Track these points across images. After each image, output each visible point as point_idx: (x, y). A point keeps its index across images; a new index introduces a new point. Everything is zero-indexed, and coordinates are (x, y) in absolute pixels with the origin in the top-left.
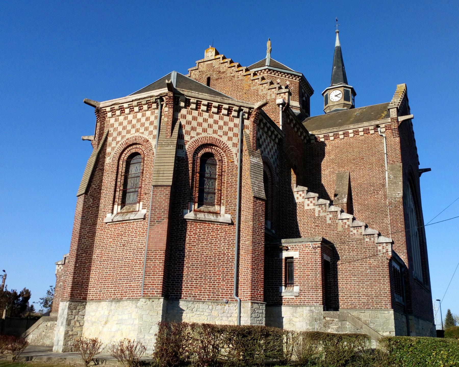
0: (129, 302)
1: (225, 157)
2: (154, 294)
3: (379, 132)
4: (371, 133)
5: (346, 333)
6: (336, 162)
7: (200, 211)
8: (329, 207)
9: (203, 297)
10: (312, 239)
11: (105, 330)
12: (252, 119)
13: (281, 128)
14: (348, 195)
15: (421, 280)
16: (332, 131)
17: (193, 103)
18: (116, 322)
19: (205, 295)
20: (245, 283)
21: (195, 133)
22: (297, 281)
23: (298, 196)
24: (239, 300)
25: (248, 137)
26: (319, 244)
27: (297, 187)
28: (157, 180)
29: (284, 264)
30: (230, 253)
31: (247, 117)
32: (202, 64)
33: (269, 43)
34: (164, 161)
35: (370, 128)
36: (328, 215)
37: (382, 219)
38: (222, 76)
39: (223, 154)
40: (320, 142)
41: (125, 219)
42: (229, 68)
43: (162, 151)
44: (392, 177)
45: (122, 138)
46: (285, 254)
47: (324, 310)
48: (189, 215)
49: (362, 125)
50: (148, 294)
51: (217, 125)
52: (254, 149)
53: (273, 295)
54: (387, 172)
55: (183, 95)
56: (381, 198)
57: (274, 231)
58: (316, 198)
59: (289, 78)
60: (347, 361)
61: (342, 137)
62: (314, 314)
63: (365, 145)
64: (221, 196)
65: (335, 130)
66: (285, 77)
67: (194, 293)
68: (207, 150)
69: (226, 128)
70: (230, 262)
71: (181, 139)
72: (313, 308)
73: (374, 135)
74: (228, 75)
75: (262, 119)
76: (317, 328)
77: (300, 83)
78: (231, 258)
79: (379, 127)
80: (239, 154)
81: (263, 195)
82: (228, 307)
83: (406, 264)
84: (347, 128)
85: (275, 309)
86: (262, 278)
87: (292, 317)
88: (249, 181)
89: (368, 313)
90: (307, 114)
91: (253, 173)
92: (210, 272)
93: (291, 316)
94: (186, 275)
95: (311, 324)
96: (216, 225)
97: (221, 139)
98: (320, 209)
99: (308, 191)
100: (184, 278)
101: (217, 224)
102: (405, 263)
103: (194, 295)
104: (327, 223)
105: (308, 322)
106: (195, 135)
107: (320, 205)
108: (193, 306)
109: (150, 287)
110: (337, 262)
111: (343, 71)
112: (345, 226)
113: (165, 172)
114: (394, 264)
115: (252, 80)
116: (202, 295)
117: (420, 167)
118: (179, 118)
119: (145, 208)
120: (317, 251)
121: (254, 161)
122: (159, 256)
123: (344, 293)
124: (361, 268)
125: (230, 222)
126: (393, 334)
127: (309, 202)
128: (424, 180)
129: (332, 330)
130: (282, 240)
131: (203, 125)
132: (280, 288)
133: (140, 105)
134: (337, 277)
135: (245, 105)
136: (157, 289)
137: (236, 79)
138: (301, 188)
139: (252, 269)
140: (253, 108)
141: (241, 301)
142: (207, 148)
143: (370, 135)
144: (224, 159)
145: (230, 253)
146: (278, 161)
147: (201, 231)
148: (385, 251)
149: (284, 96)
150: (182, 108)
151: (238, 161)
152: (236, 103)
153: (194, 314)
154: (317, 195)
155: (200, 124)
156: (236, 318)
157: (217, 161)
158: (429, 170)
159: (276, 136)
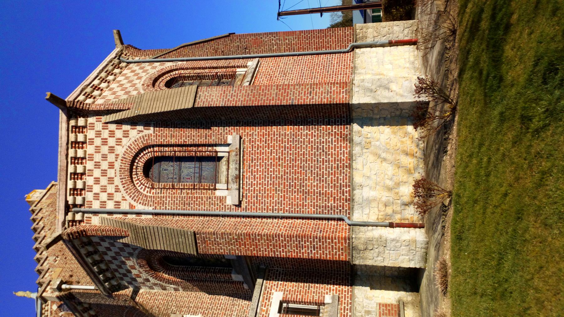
33: (20, 294)
45: (117, 190)
97: (121, 155)
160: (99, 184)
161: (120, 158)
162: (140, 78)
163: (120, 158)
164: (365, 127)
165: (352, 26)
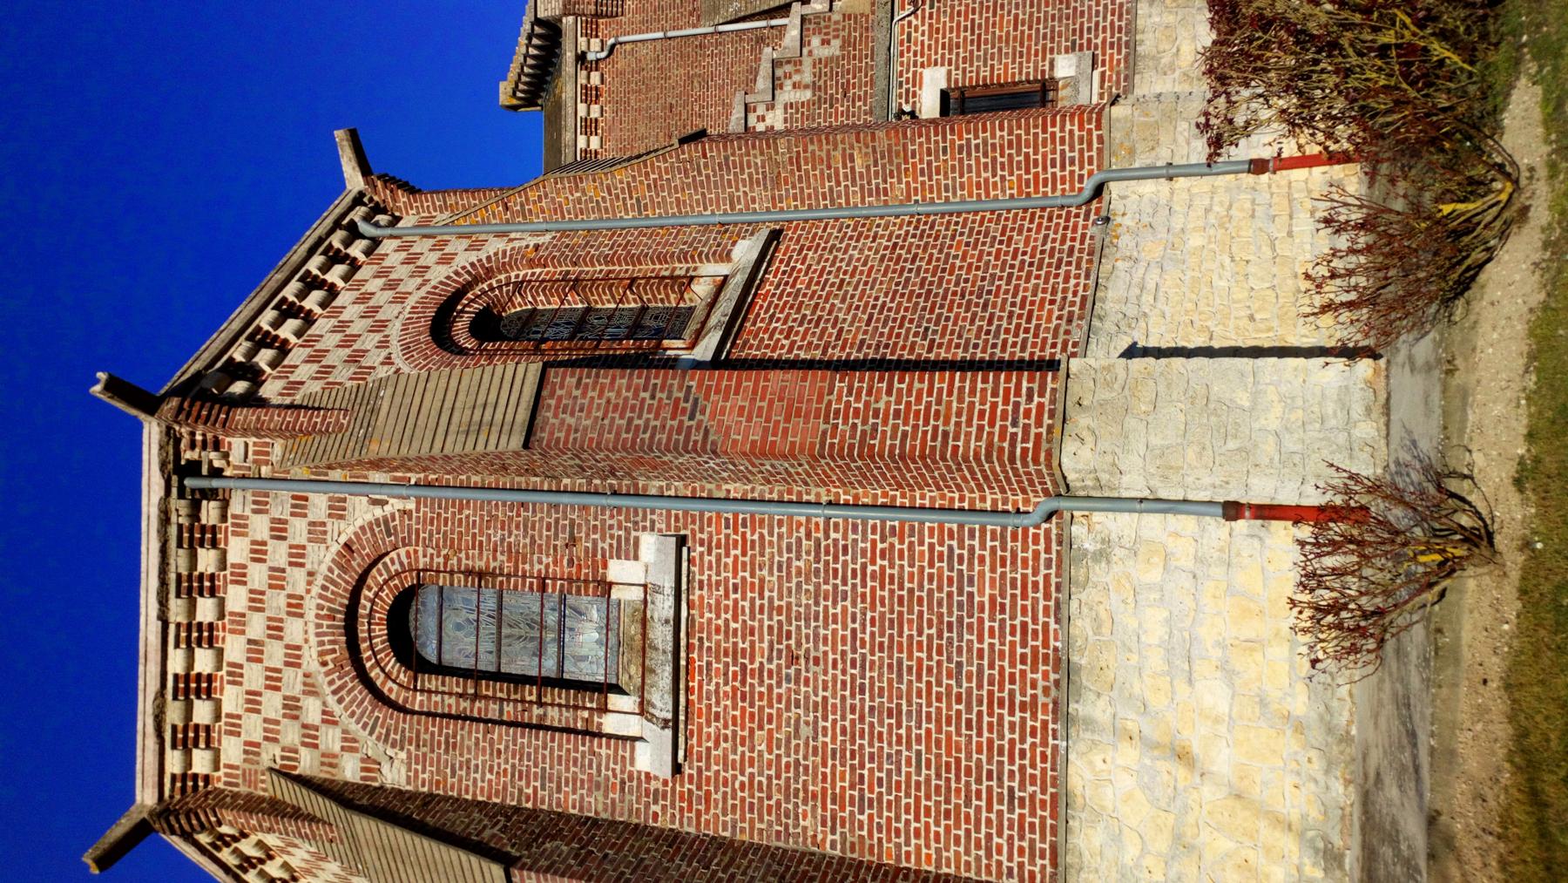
0: (1074, 604)
2: (1041, 406)
11: (1222, 760)
18: (1182, 688)
22: (1036, 63)
28: (506, 428)
34: (434, 414)
35: (582, 80)
36: (810, 53)
41: (670, 648)
43: (387, 436)
45: (311, 690)
50: (1038, 436)
79: (584, 54)
98: (788, 85)
107: (776, 84)
109: (1003, 429)
113: (481, 401)
119: (637, 539)
122: (858, 399)
133: (195, 586)
136: (1018, 394)
161: (320, 581)
162: (400, 299)
163: (320, 581)
165: (1249, 171)
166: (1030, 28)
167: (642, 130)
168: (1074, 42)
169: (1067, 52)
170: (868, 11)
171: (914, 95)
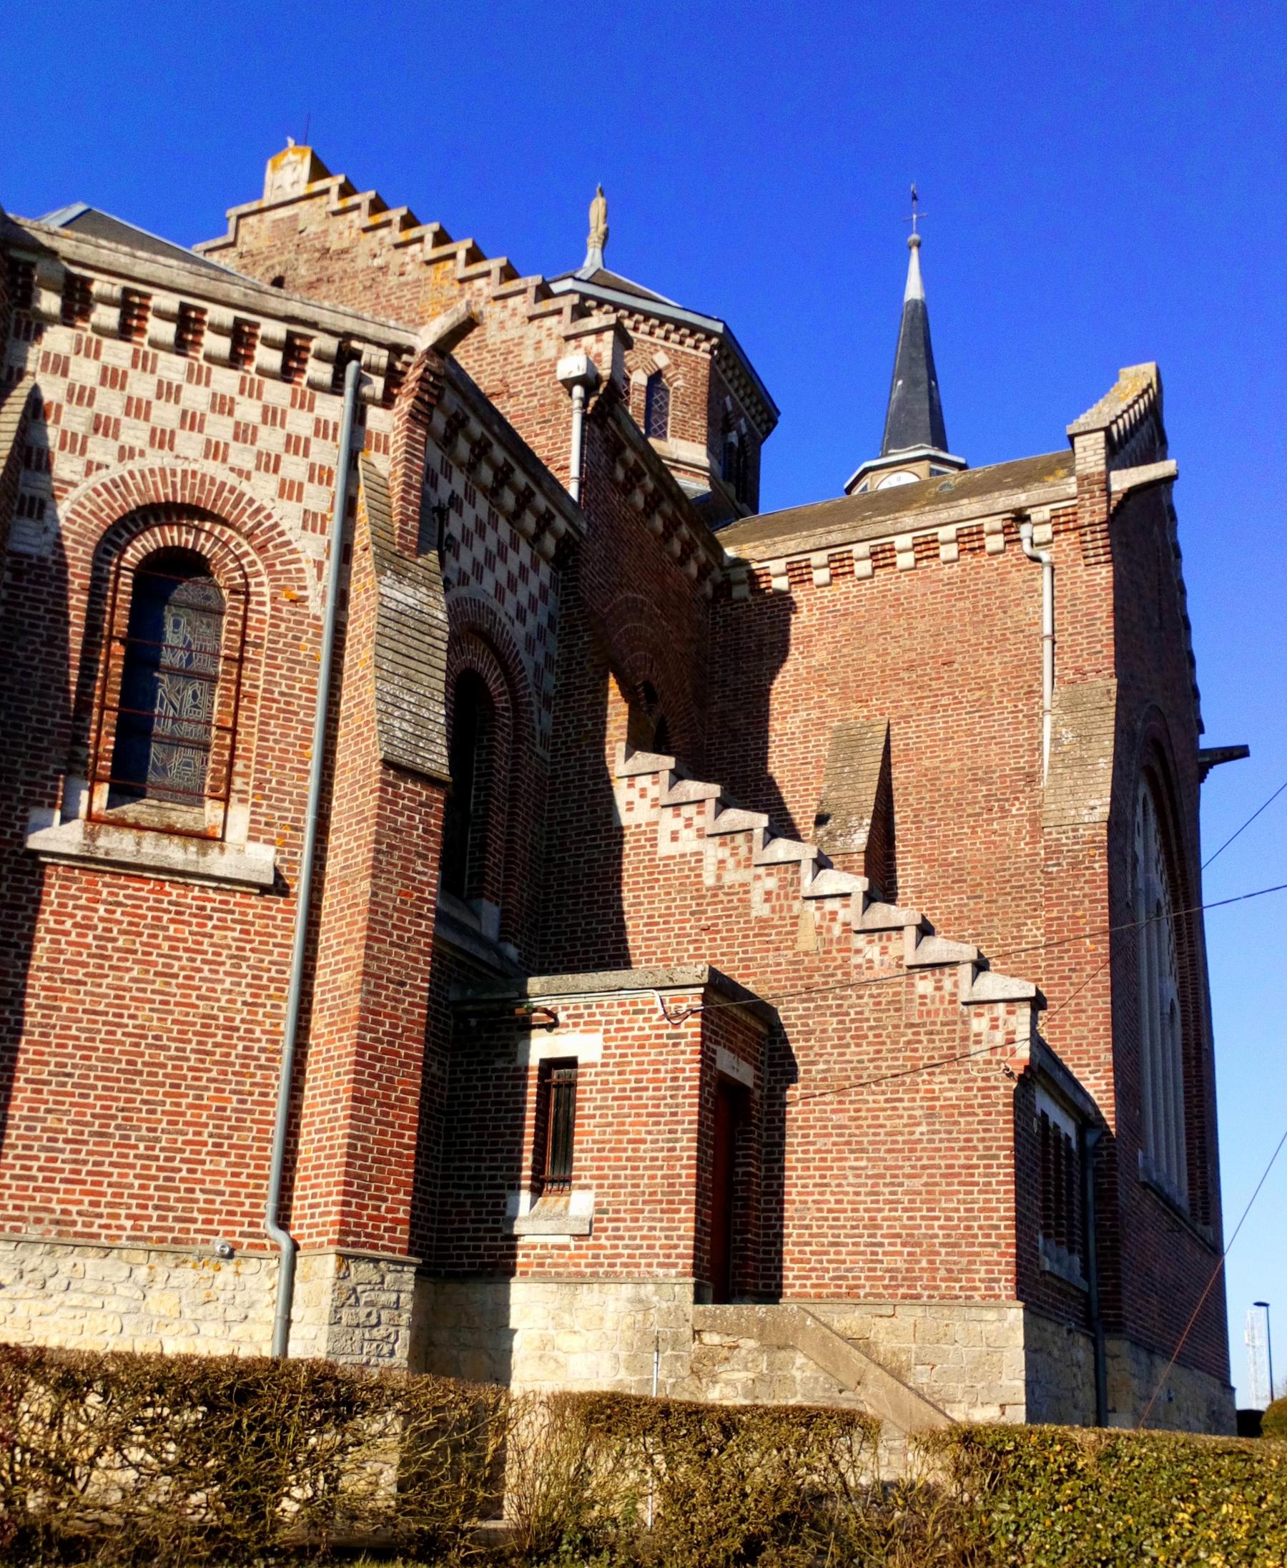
1: (264, 579)
3: (1026, 543)
4: (989, 548)
5: (792, 1402)
6: (834, 679)
7: (120, 824)
8: (765, 844)
9: (108, 1227)
10: (662, 977)
12: (404, 404)
13: (573, 490)
14: (874, 818)
15: (1183, 1201)
16: (824, 543)
17: (107, 301)
19: (117, 1216)
20: (321, 1167)
21: (113, 446)
23: (633, 795)
24: (286, 1246)
25: (380, 489)
26: (693, 999)
27: (628, 755)
29: (532, 1091)
30: (259, 1023)
31: (379, 393)
32: (252, 220)
33: (597, 207)
36: (758, 877)
37: (1018, 926)
38: (336, 267)
39: (252, 564)
40: (771, 596)
42: (366, 230)
44: (1068, 735)
46: (541, 1046)
47: (699, 1299)
48: (56, 836)
49: (953, 514)
51: (229, 422)
52: (406, 548)
53: (477, 1230)
54: (1048, 720)
55: (52, 254)
56: (1018, 831)
57: (512, 951)
58: (710, 806)
59: (666, 338)
60: (753, 1546)
61: (863, 568)
62: (654, 1316)
63: (960, 605)
64: (232, 756)
65: (836, 538)
66: (651, 333)
67: (58, 1208)
68: (175, 536)
69: (271, 440)
70: (260, 1067)
71: (38, 468)
72: (651, 1288)
73: (1001, 557)
74: (361, 263)
75: (454, 411)
76: (661, 1380)
77: (714, 363)
78: (262, 1050)
79: (1027, 519)
80: (330, 567)
81: (437, 759)
82: (231, 1278)
83: (1108, 1114)
84: (888, 526)
85: (481, 1293)
86: (408, 1147)
87: (552, 1332)
88: (369, 692)
89: (908, 1316)
90: (744, 507)
91: (390, 655)
92: (153, 1112)
93: (551, 1324)
94: (23, 1118)
95: (634, 1363)
96: (196, 892)
97: (244, 486)
98: (724, 853)
99: (677, 776)
100: (14, 1133)
101: (203, 888)
102: (1104, 1111)
103: (57, 1216)
104: (754, 914)
105: (623, 1354)
106: (111, 459)
107: (726, 836)
108: (47, 1267)
110: (784, 1089)
111: (931, 398)
112: (829, 930)
114: (1044, 1103)
115: (462, 281)
116: (100, 1216)
117: (1207, 741)
118: (30, 367)
120: (682, 1030)
121: (400, 597)
123: (808, 1227)
124: (889, 1118)
125: (269, 879)
126: (1018, 1415)
127: (679, 824)
128: (1219, 796)
129: (729, 1391)
130: (531, 980)
131: (154, 412)
132: (510, 1199)
134: (781, 1159)
135: (370, 330)
137: (393, 280)
138: (645, 760)
139: (354, 1099)
140: (411, 351)
141: (296, 1247)
142: (171, 525)
143: (984, 559)
144: (261, 584)
145: (259, 1023)
146: (552, 640)
147: (118, 915)
148: (999, 1038)
149: (596, 348)
150: (50, 320)
151: (323, 598)
152: (326, 319)
153: (50, 1305)
154: (714, 790)
155: (138, 409)
156: (269, 1330)
157: (225, 592)
158: (1240, 752)
159: (545, 522)
160: (103, 383)
164: (512, 1326)
166: (628, 1159)
167: (921, 625)
168: (605, 1212)
169: (597, 1204)
170: (799, 947)
171: (576, 1025)
